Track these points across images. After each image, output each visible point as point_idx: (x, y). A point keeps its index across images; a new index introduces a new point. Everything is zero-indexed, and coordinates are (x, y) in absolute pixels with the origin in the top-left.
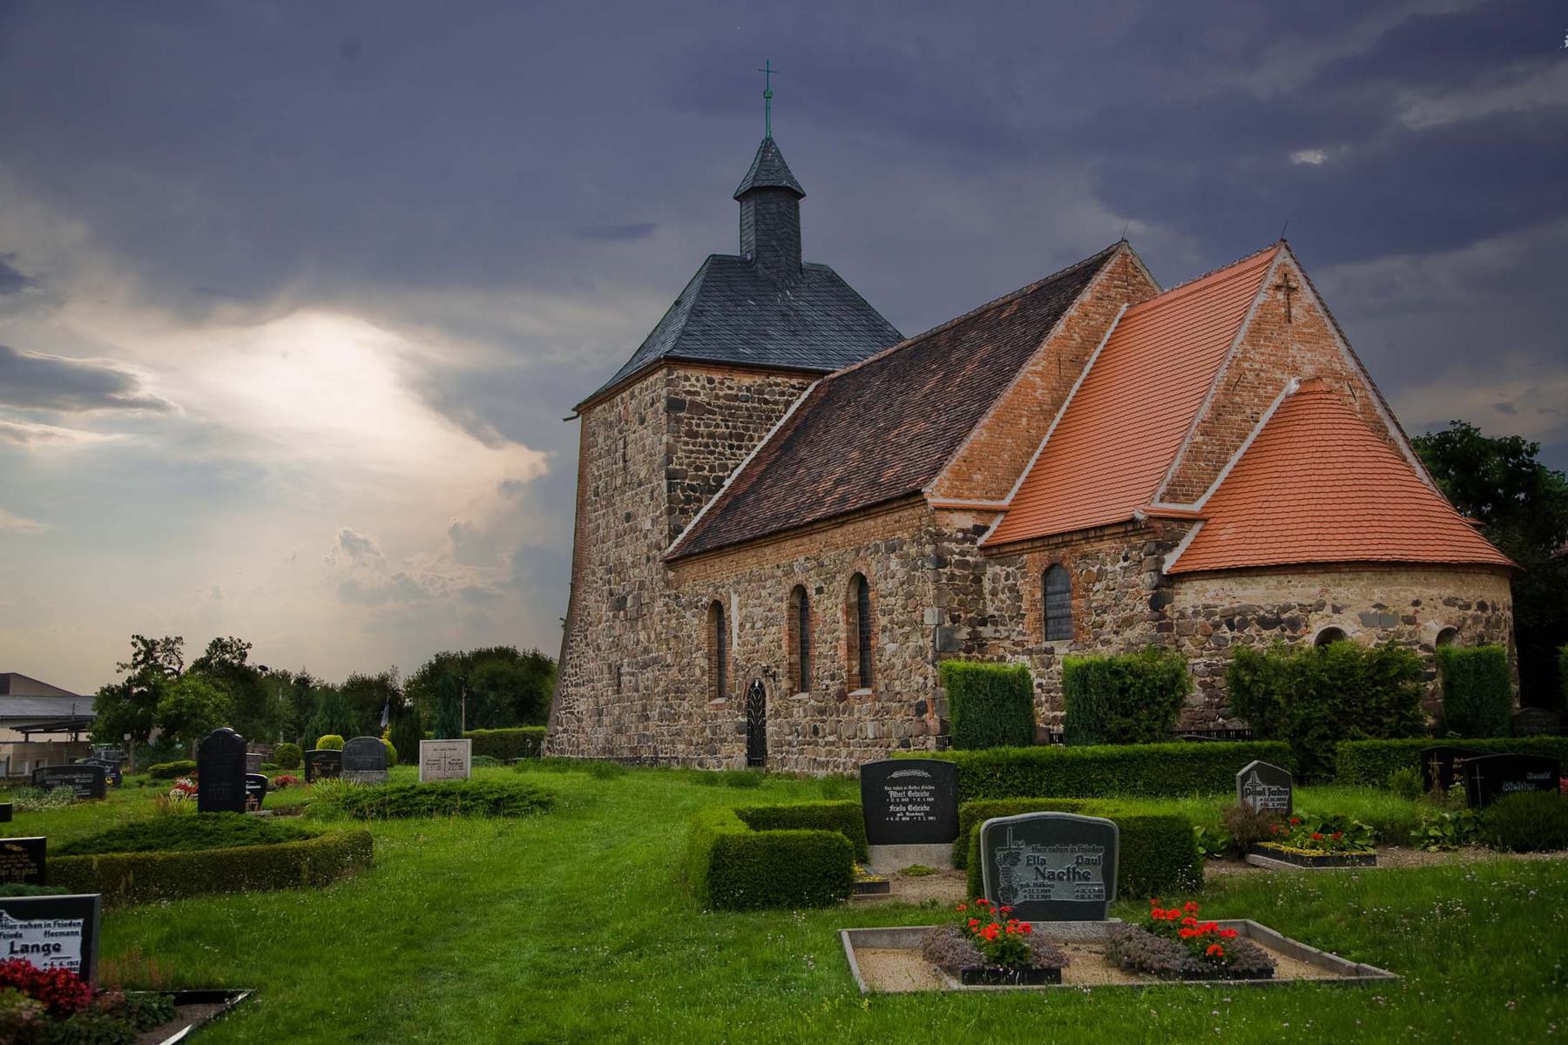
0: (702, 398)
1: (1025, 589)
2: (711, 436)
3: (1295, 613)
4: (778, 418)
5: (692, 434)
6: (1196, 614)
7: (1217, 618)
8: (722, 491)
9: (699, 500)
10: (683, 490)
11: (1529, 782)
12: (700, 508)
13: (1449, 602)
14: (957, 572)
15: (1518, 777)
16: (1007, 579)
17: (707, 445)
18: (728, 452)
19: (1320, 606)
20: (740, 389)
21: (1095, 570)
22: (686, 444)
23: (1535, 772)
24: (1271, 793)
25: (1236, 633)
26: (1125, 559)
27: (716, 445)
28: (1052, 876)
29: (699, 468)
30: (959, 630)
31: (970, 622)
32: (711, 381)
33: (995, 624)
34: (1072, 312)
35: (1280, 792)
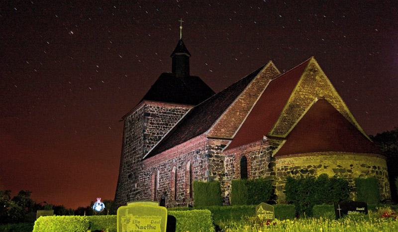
1: (235, 164)
2: (158, 124)
7: (289, 170)
9: (153, 143)
10: (148, 140)
11: (357, 211)
12: (154, 146)
13: (363, 166)
15: (354, 209)
16: (230, 161)
17: (156, 127)
20: (167, 110)
21: (253, 156)
22: (150, 126)
24: (267, 213)
25: (294, 175)
28: (142, 228)
31: (220, 175)
32: (158, 108)
33: (227, 175)
35: (270, 213)
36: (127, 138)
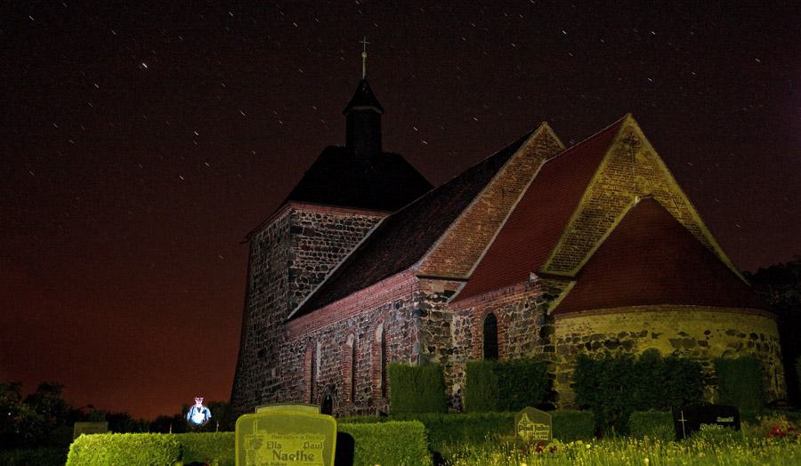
0: (313, 225)
2: (318, 249)
3: (628, 338)
4: (360, 239)
5: (305, 248)
6: (568, 340)
7: (581, 342)
8: (323, 282)
9: (308, 288)
10: (299, 281)
11: (719, 424)
13: (730, 333)
14: (433, 320)
15: (712, 421)
17: (315, 255)
18: (328, 259)
19: (644, 334)
20: (336, 222)
22: (302, 253)
23: (723, 417)
24: (537, 429)
26: (527, 306)
27: (320, 255)
29: (309, 268)
30: (434, 356)
31: (442, 351)
32: (318, 216)
34: (511, 162)
35: (543, 429)
36: (256, 278)
